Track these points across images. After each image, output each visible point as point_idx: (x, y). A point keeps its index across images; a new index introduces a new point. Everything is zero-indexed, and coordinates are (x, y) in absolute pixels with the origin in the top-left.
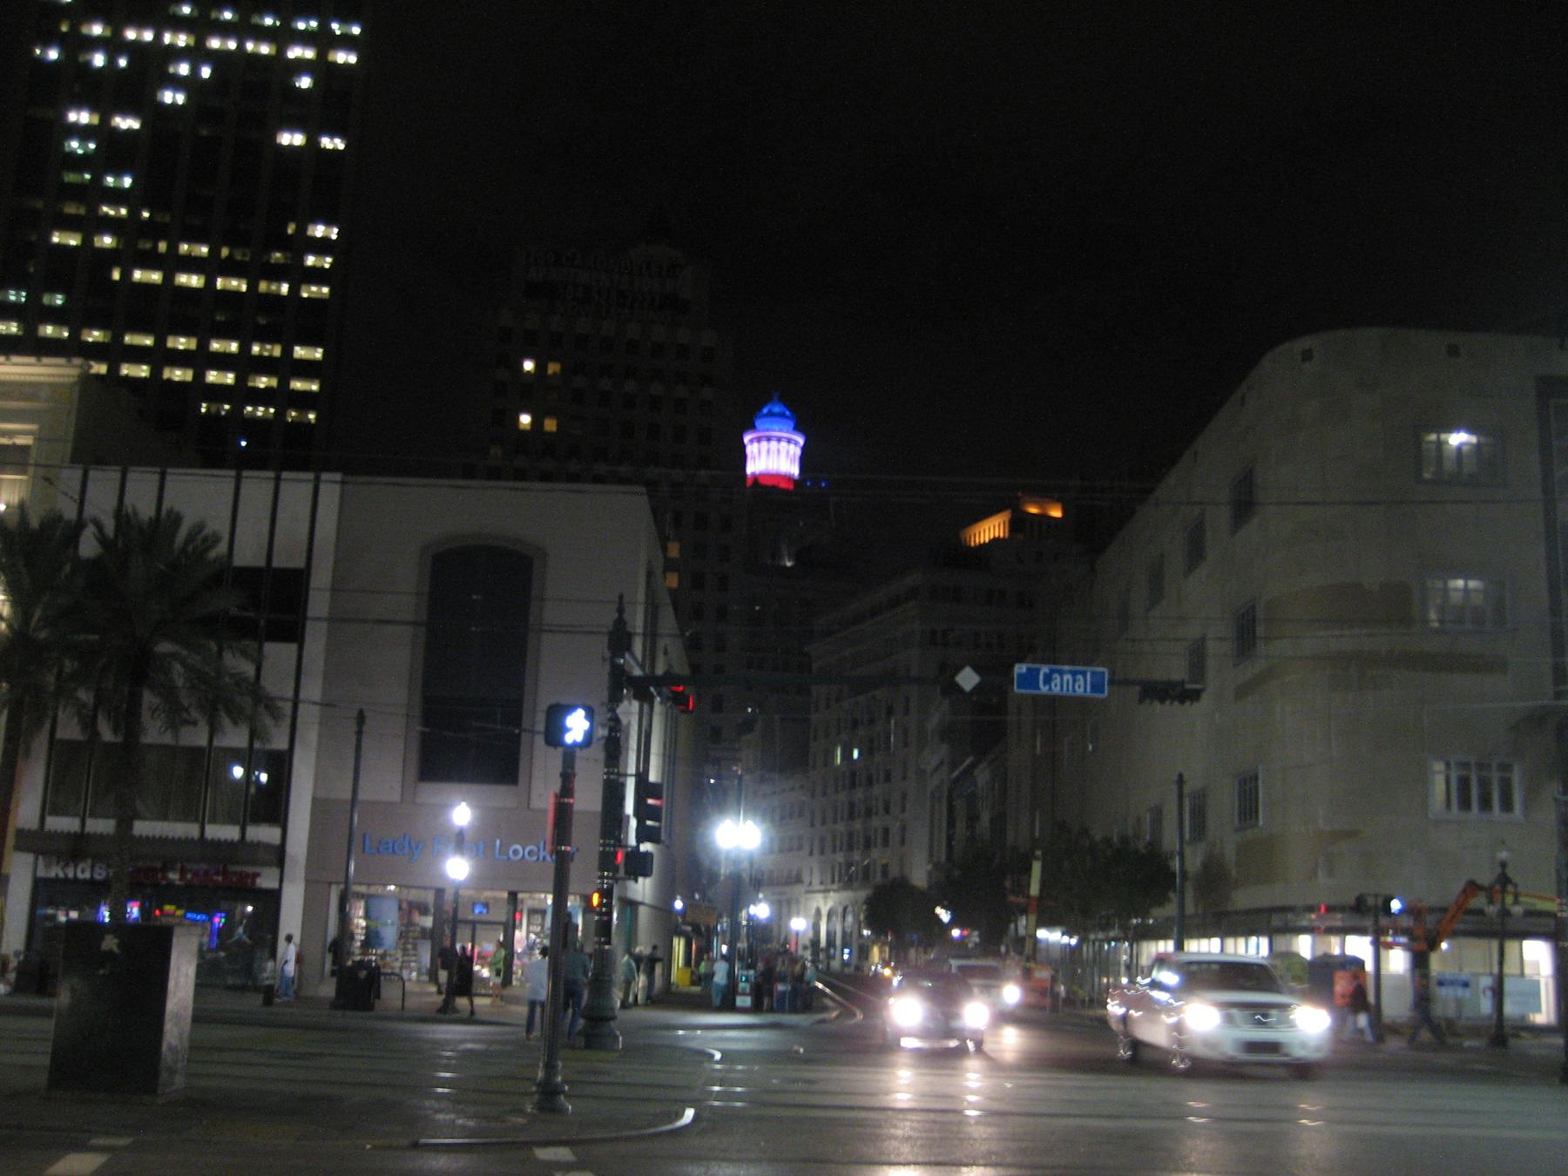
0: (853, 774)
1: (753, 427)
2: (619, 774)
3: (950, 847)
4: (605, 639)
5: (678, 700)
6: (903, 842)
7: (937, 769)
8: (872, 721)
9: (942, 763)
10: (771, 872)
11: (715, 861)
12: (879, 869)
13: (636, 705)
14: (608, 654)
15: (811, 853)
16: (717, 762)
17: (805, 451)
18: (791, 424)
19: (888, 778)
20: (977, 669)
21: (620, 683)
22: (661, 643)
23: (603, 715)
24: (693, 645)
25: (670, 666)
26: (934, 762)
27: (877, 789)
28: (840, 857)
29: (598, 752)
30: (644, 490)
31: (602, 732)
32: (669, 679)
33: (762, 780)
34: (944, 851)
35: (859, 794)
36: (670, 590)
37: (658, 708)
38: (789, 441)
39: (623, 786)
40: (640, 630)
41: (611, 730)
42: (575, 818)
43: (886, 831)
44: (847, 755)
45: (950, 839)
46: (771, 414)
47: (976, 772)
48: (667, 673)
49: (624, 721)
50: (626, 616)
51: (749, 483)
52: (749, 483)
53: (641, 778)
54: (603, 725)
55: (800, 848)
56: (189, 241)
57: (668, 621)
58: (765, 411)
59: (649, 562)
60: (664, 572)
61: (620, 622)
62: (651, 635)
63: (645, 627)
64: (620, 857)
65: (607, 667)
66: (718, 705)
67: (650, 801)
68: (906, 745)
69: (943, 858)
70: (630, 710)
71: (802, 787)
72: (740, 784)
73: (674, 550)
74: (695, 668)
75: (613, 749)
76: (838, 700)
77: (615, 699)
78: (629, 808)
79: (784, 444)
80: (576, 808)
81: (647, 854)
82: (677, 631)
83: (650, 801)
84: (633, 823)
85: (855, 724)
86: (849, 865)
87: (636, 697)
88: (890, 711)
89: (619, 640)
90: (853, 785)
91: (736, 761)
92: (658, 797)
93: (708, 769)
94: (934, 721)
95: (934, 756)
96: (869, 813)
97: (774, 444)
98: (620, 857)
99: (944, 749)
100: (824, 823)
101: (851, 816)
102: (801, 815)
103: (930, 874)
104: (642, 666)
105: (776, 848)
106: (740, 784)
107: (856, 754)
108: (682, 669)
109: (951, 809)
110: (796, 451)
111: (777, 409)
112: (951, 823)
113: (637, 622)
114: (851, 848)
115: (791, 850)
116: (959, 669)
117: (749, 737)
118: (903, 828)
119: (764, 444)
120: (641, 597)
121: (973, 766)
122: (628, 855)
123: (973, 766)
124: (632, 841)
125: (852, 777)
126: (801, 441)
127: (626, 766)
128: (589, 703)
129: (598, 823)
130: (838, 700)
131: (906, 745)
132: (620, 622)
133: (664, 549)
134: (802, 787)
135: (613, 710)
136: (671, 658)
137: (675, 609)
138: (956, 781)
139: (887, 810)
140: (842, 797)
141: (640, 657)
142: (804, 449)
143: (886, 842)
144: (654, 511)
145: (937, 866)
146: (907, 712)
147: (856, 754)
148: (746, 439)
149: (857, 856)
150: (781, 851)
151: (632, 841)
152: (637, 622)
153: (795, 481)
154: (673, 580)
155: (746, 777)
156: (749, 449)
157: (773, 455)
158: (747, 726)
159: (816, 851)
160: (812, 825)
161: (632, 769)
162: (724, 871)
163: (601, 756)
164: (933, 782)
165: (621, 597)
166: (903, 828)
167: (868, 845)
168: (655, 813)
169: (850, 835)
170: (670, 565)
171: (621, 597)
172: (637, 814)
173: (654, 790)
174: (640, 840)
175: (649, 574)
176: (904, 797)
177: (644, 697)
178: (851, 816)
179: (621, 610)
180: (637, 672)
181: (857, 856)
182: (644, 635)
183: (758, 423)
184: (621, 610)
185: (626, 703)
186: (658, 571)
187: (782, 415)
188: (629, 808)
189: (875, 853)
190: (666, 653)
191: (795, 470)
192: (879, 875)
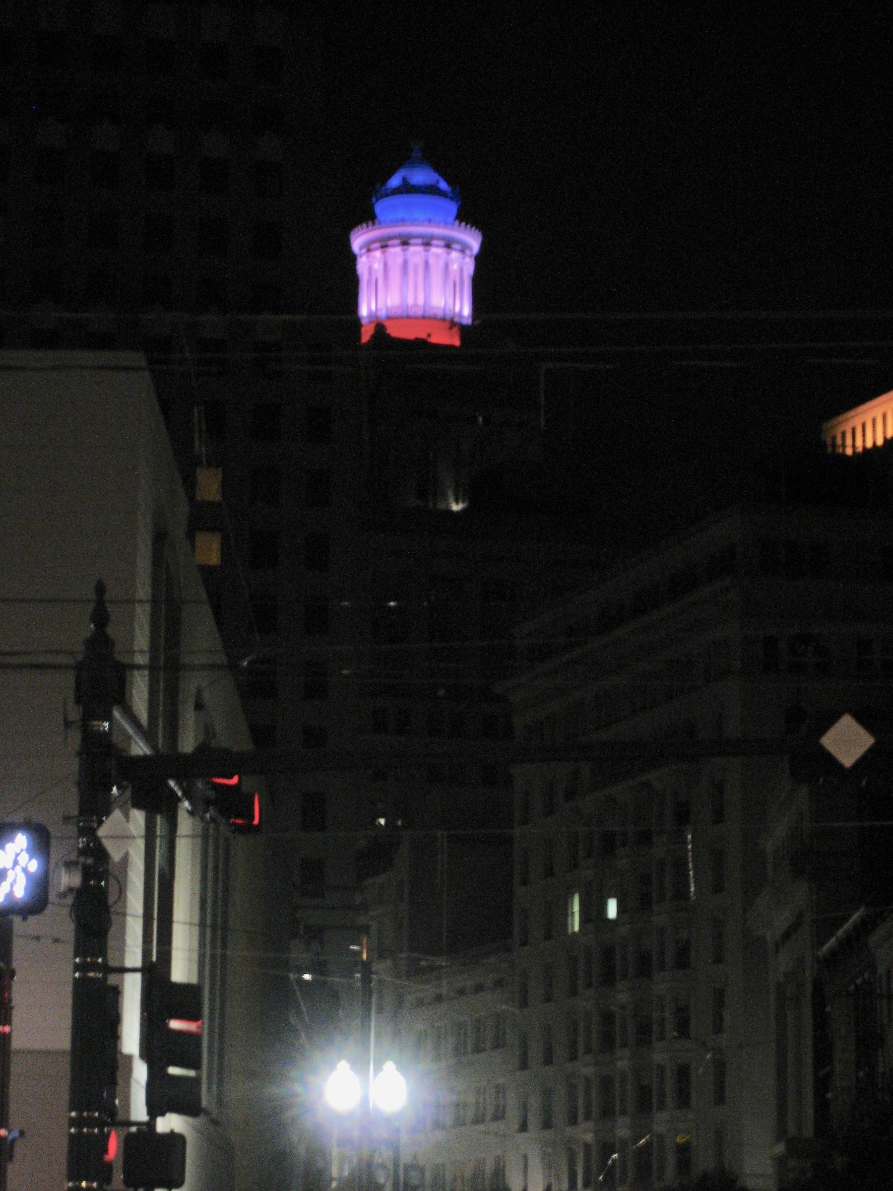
0: (608, 953)
1: (368, 216)
2: (107, 969)
3: (822, 1106)
4: (69, 679)
5: (226, 807)
6: (720, 1098)
7: (787, 936)
8: (645, 838)
9: (796, 926)
10: (438, 1171)
11: (318, 1152)
12: (671, 1159)
13: (138, 817)
14: (75, 713)
15: (523, 1128)
16: (315, 934)
17: (485, 264)
18: (453, 208)
19: (682, 960)
20: (865, 719)
21: (104, 775)
22: (191, 684)
23: (67, 844)
24: (255, 688)
25: (208, 730)
26: (782, 919)
27: (662, 984)
28: (585, 1133)
29: (60, 922)
30: (138, 358)
31: (68, 880)
32: (208, 760)
33: (415, 972)
34: (810, 1112)
35: (622, 995)
36: (206, 571)
37: (185, 824)
38: (448, 245)
39: (116, 992)
40: (141, 659)
41: (87, 874)
42: (16, 1067)
43: (683, 1073)
44: (593, 912)
45: (822, 1085)
46: (407, 189)
47: (873, 939)
48: (202, 749)
49: (116, 855)
50: (111, 631)
51: (366, 337)
52: (366, 337)
53: (155, 972)
54: (69, 865)
55: (500, 1115)
56: (99, 978)
57: (202, 638)
58: (395, 181)
59: (194, 551)
60: (191, 536)
61: (100, 645)
62: (168, 668)
63: (154, 648)
64: (114, 1147)
65: (75, 738)
66: (314, 813)
67: (175, 1024)
68: (718, 888)
69: (809, 1131)
70: (126, 832)
71: (499, 983)
72: (366, 980)
73: (210, 486)
74: (261, 735)
75: (94, 914)
76: (570, 794)
77: (94, 807)
78: (131, 1039)
79: (437, 251)
80: (16, 1043)
81: (175, 1140)
82: (221, 658)
83: (175, 1024)
84: (140, 1072)
85: (610, 844)
86: (607, 1149)
87: (137, 804)
88: (683, 816)
89: (100, 682)
90: (609, 977)
91: (359, 932)
92: (192, 1015)
93: (297, 953)
94: (777, 834)
95: (780, 911)
96: (645, 1034)
97: (416, 251)
98: (114, 1147)
99: (801, 894)
100: (548, 1060)
101: (608, 1043)
102: (498, 1044)
103: (780, 1161)
104: (149, 736)
105: (448, 1120)
106: (366, 980)
107: (612, 909)
108: (233, 737)
109: (821, 1023)
110: (463, 265)
111: (421, 176)
112: (823, 1054)
113: (138, 640)
114: (607, 1113)
115: (478, 1120)
116: (828, 720)
117: (381, 878)
118: (720, 1067)
119: (396, 251)
120: (143, 590)
121: (865, 927)
122: (130, 1142)
123: (865, 927)
124: (139, 1111)
125: (606, 961)
126: (473, 241)
127: (122, 949)
128: (37, 819)
129: (63, 1069)
130: (570, 794)
131: (718, 888)
132: (100, 645)
133: (190, 483)
134: (499, 983)
135: (90, 832)
136: (209, 715)
137: (217, 612)
138: (831, 960)
139: (683, 1029)
140: (586, 1003)
141: (143, 716)
142: (481, 260)
143: (683, 1099)
144: (166, 407)
145: (795, 1147)
146: (719, 817)
147: (612, 909)
148: (358, 241)
149: (622, 1130)
150: (459, 1122)
151: (139, 1111)
152: (138, 640)
153: (464, 331)
154: (209, 549)
155: (382, 968)
156: (362, 266)
157: (416, 275)
158: (377, 856)
159: (534, 1121)
160: (524, 1065)
161: (134, 957)
162: (273, 1090)
163: (67, 929)
164: (783, 963)
165: (100, 589)
166: (720, 1067)
167: (645, 1102)
168: (186, 1050)
169: (606, 1083)
170: (201, 519)
171: (100, 589)
172: (147, 1053)
173: (185, 1000)
174: (156, 1108)
175: (160, 538)
176: (719, 997)
177: (157, 804)
178: (608, 1043)
179: (101, 618)
180: (140, 748)
181: (622, 1130)
182: (152, 668)
183: (381, 207)
184: (101, 618)
185: (117, 814)
186: (179, 532)
187: (431, 190)
188: (131, 1039)
189: (661, 1121)
190: (199, 706)
191: (464, 309)
192: (670, 1172)
